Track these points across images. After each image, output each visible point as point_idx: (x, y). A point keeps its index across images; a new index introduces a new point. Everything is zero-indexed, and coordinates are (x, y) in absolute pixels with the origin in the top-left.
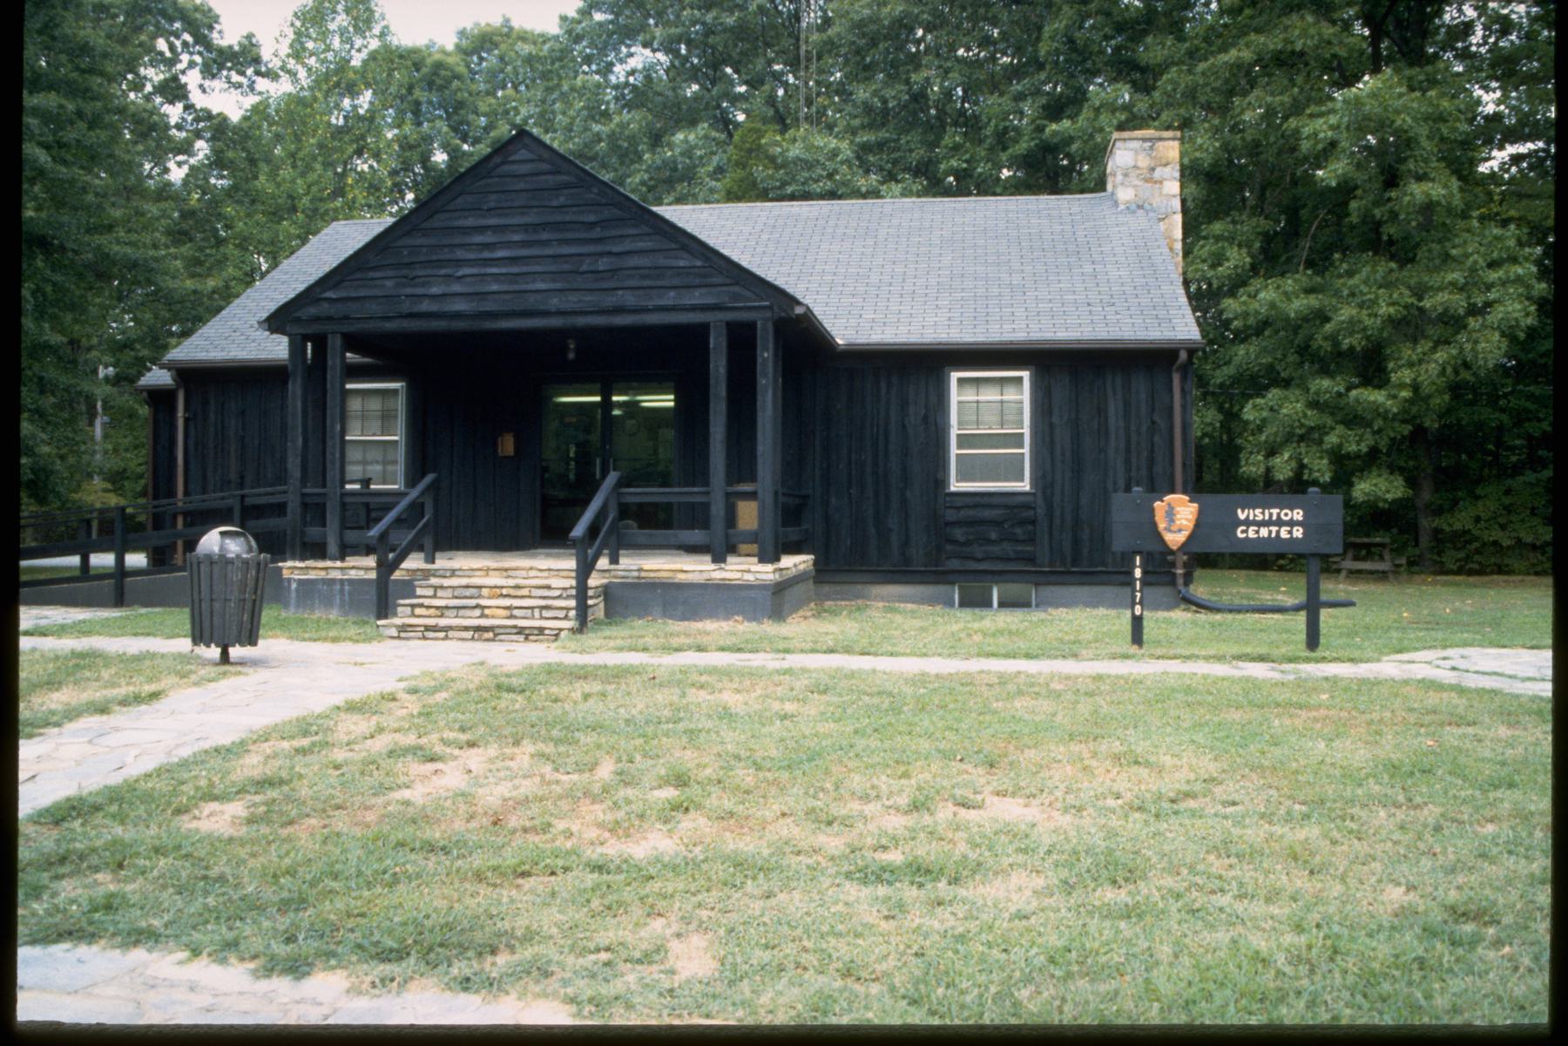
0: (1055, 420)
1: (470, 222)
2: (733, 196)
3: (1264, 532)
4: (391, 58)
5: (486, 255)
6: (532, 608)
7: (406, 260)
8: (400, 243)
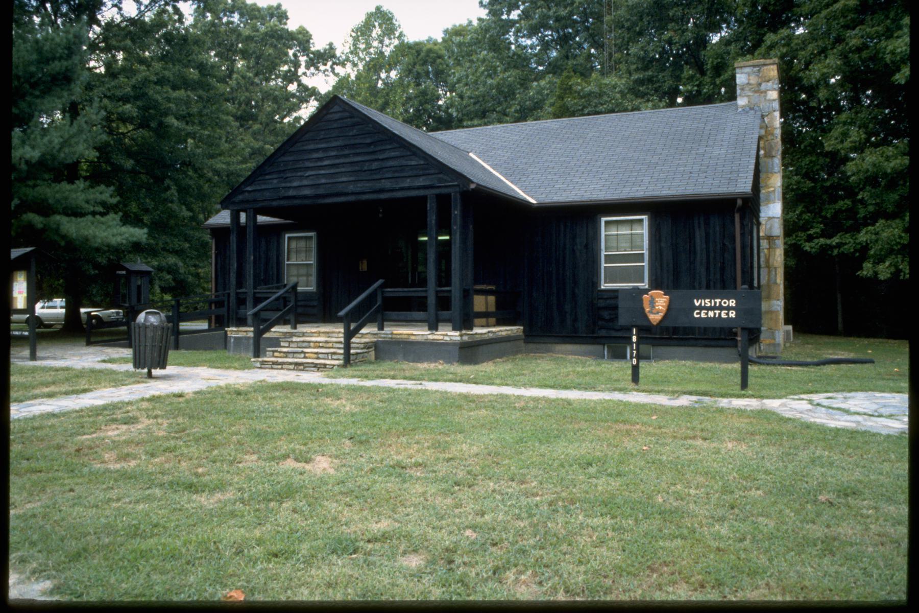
0: (663, 245)
1: (312, 147)
2: (557, 116)
3: (711, 314)
4: (405, 49)
5: (319, 164)
6: (327, 354)
7: (282, 169)
8: (280, 160)
